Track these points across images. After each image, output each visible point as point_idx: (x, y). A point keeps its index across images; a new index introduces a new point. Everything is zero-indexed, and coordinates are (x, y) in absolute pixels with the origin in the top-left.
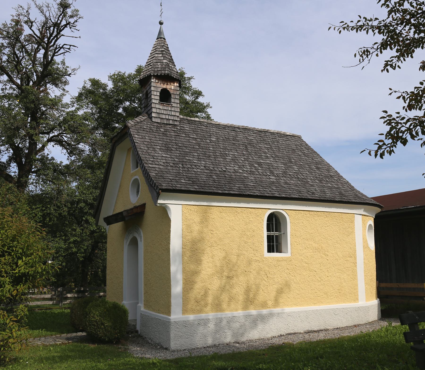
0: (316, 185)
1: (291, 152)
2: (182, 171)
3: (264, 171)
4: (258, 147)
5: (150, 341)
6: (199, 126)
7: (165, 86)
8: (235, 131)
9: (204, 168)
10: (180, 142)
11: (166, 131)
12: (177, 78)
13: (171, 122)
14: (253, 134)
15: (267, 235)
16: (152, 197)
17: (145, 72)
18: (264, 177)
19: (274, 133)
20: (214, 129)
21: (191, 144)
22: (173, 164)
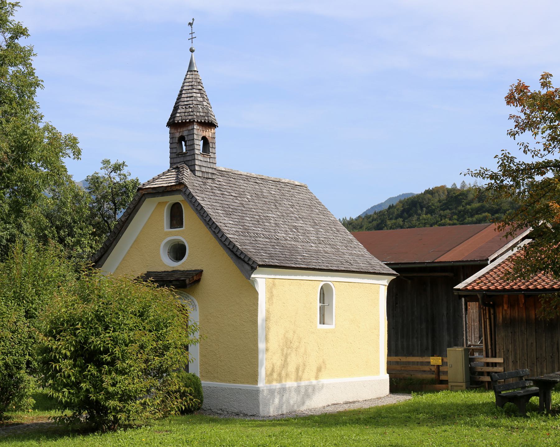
8: (257, 183)
13: (210, 176)
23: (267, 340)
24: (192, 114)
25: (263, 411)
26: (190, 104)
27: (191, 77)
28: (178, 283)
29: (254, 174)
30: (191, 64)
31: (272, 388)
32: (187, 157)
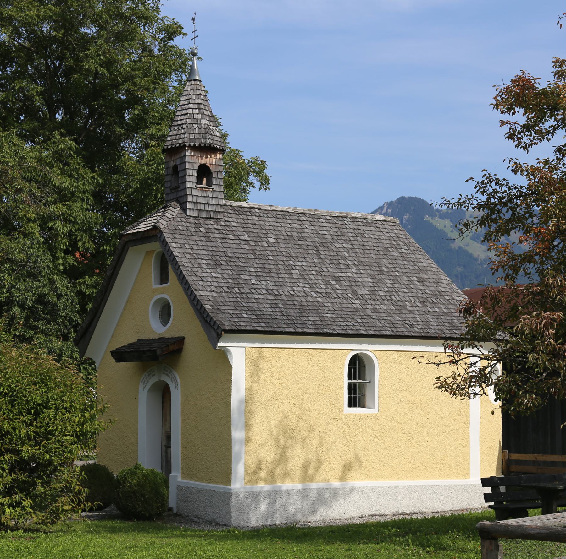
0: (417, 311)
1: (381, 253)
2: (241, 298)
3: (344, 291)
4: (335, 249)
5: (195, 519)
6: (250, 217)
7: (203, 161)
8: (300, 220)
9: (266, 292)
10: (229, 250)
11: (208, 230)
12: (221, 148)
13: (212, 215)
14: (326, 225)
15: (349, 384)
16: (209, 338)
17: (174, 137)
18: (344, 301)
19: (356, 218)
20: (270, 220)
21: (243, 251)
22: (228, 288)
23: (247, 426)
24: (183, 136)
25: (235, 519)
26: (183, 124)
27: (189, 88)
29: (300, 208)
31: (254, 490)
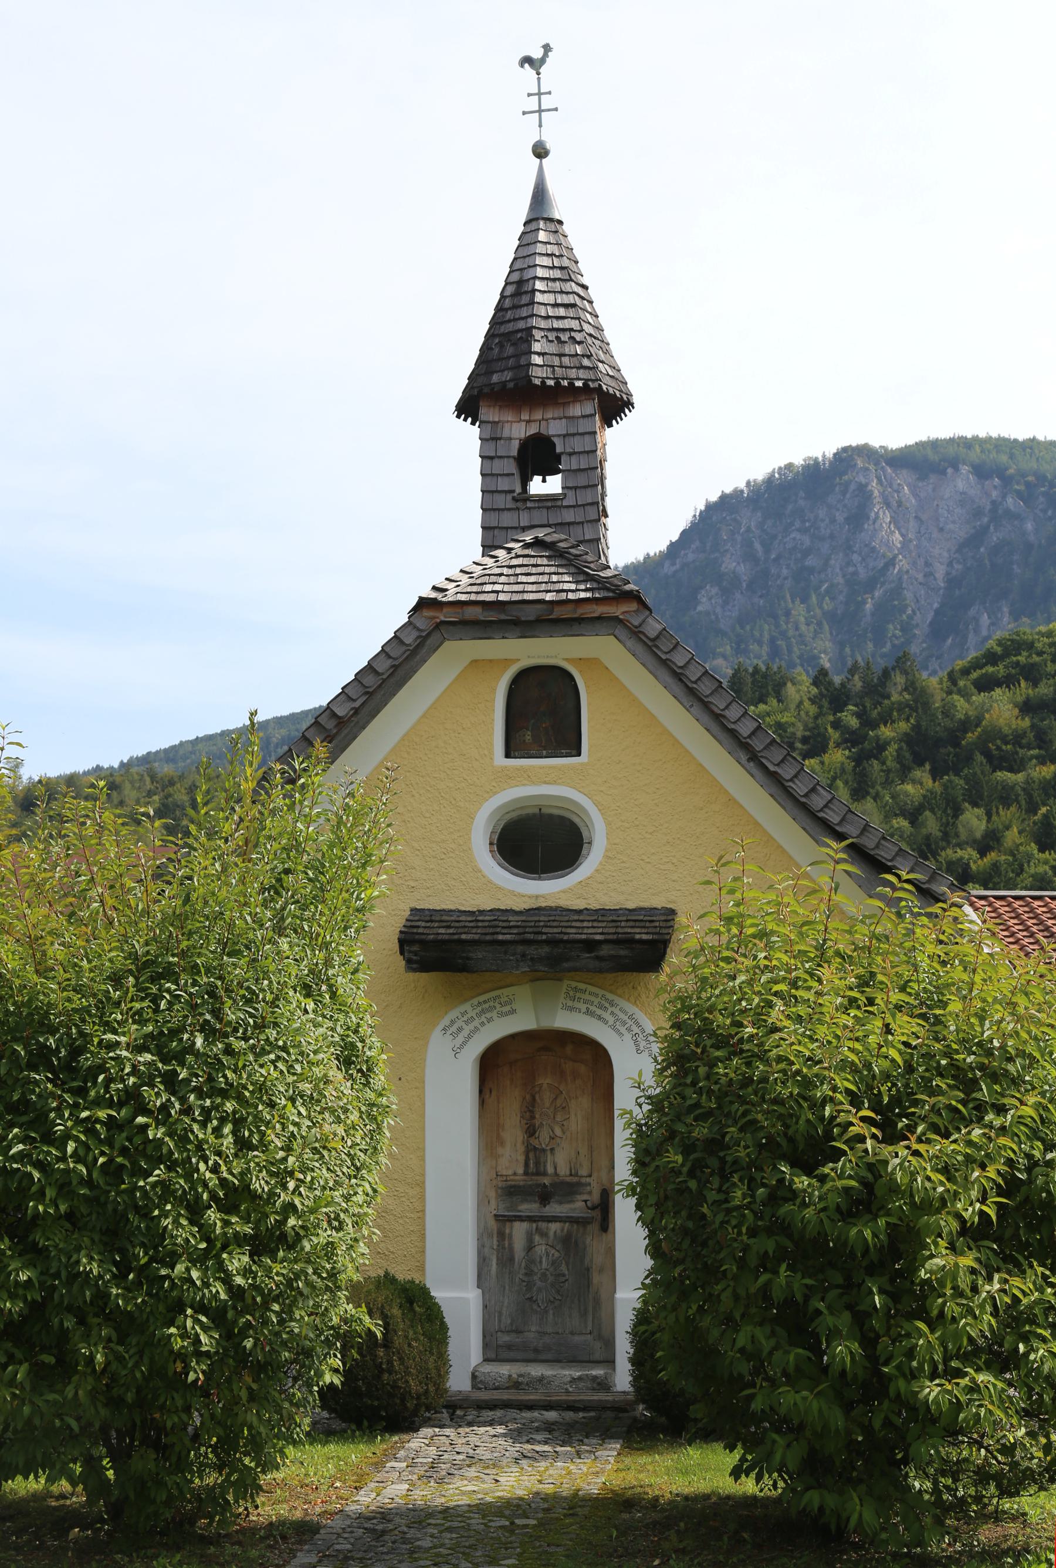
28: (622, 953)
30: (540, 196)
32: (564, 511)
